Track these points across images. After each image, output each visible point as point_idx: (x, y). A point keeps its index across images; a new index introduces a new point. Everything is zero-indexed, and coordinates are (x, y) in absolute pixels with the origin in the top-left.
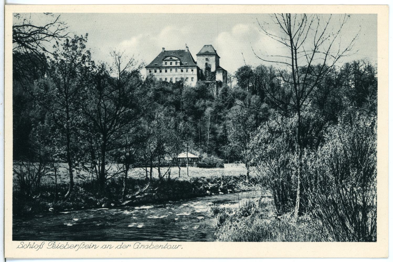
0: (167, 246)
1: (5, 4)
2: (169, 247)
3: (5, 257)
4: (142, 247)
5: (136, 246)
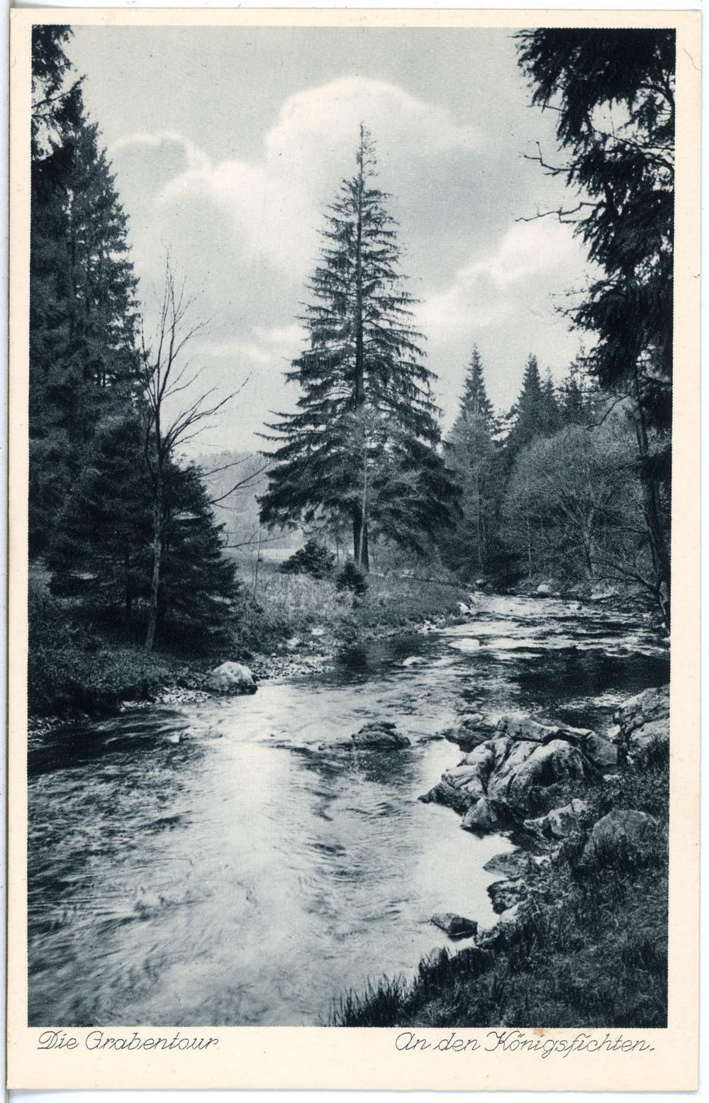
0: (177, 1042)
1: (13, 5)
2: (183, 1044)
3: (9, 1087)
4: (110, 1044)
5: (92, 1043)
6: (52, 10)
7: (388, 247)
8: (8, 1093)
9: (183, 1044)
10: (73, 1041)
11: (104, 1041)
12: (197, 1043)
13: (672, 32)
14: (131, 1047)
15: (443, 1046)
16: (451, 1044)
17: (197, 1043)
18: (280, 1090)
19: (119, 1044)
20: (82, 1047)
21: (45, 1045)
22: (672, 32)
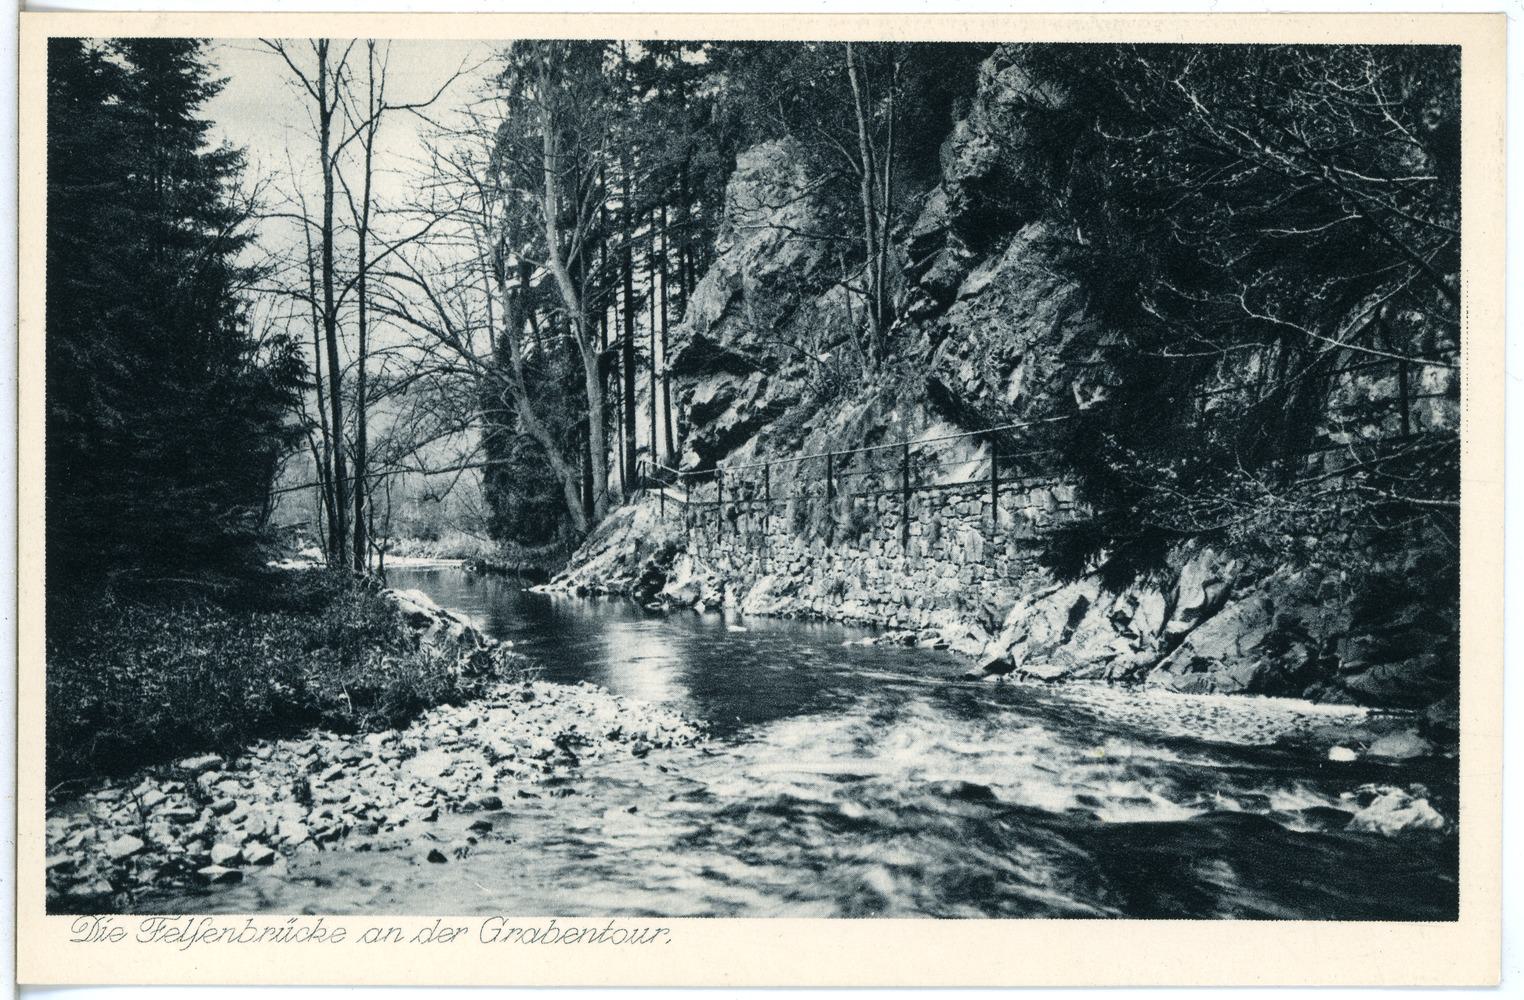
1: (23, 7)
2: (619, 937)
3: (19, 982)
4: (515, 936)
5: (488, 934)
6: (61, 15)
7: (299, 200)
8: (19, 989)
9: (619, 937)
10: (119, 931)
11: (505, 931)
12: (639, 934)
13: (1458, 48)
14: (546, 939)
15: (371, 936)
16: (436, 934)
17: (639, 934)
18: (346, 986)
19: (530, 935)
20: (130, 939)
21: (83, 936)
22: (1458, 48)
